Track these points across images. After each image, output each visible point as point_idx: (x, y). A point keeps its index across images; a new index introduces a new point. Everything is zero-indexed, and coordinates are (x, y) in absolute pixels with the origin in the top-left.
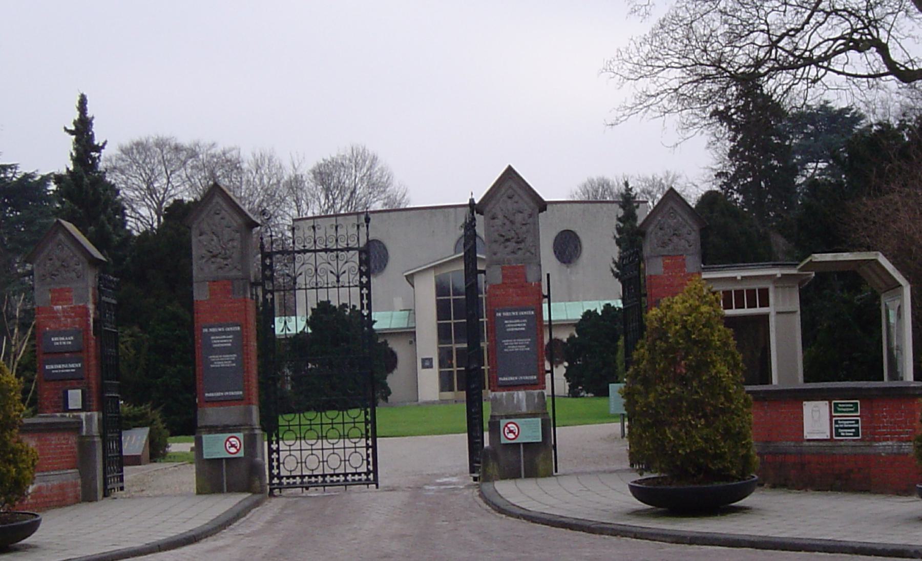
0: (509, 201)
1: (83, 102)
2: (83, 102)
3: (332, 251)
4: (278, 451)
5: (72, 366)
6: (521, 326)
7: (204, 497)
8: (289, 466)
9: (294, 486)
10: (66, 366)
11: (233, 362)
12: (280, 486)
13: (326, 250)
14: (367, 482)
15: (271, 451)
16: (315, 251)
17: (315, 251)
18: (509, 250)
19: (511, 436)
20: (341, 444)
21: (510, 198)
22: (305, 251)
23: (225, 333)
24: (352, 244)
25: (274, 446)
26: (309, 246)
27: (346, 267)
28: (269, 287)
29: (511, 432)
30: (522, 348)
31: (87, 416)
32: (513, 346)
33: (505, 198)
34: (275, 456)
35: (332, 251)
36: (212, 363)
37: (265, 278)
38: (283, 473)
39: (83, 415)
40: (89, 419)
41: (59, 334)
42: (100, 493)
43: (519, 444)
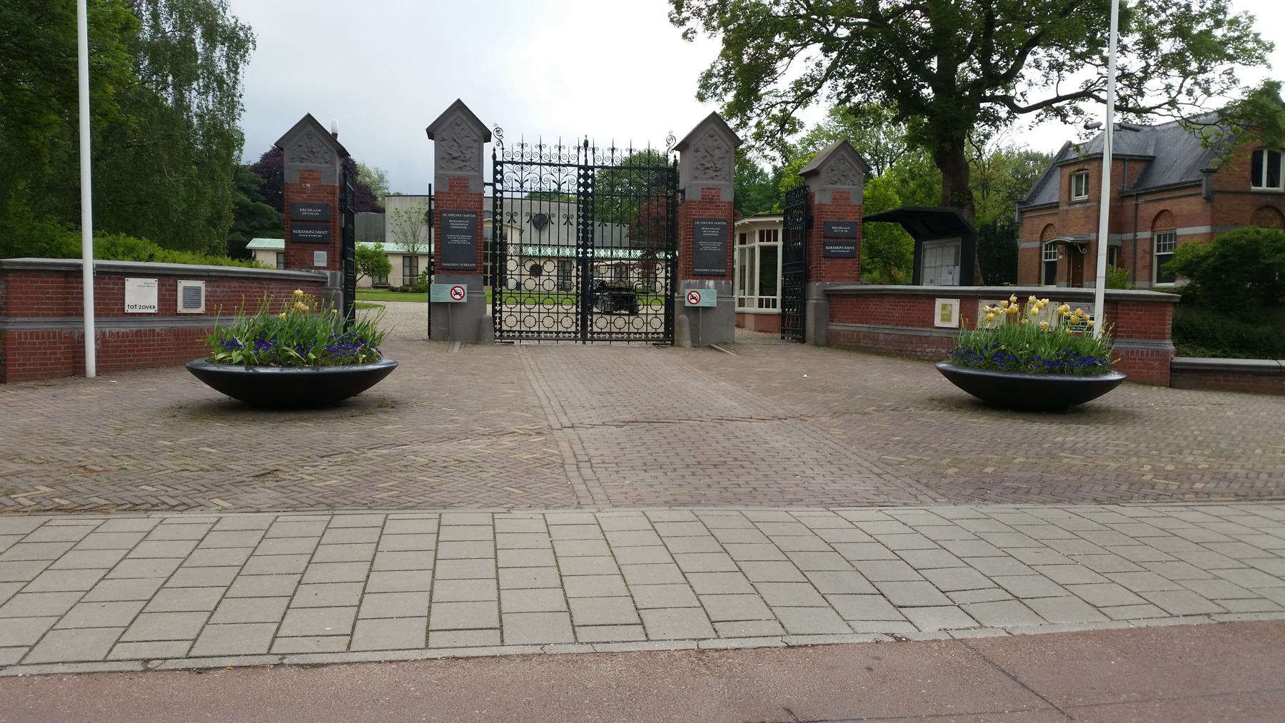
1: (1269, 67)
2: (1269, 67)
3: (517, 163)
4: (501, 311)
6: (463, 225)
7: (435, 344)
8: (510, 322)
9: (622, 340)
13: (550, 164)
14: (576, 339)
15: (494, 311)
16: (541, 164)
17: (541, 164)
22: (531, 163)
23: (462, 218)
24: (573, 162)
25: (498, 308)
26: (536, 160)
27: (566, 179)
28: (499, 186)
30: (715, 249)
32: (706, 246)
34: (498, 315)
35: (517, 163)
37: (495, 180)
38: (573, 329)
39: (328, 273)
41: (837, 224)
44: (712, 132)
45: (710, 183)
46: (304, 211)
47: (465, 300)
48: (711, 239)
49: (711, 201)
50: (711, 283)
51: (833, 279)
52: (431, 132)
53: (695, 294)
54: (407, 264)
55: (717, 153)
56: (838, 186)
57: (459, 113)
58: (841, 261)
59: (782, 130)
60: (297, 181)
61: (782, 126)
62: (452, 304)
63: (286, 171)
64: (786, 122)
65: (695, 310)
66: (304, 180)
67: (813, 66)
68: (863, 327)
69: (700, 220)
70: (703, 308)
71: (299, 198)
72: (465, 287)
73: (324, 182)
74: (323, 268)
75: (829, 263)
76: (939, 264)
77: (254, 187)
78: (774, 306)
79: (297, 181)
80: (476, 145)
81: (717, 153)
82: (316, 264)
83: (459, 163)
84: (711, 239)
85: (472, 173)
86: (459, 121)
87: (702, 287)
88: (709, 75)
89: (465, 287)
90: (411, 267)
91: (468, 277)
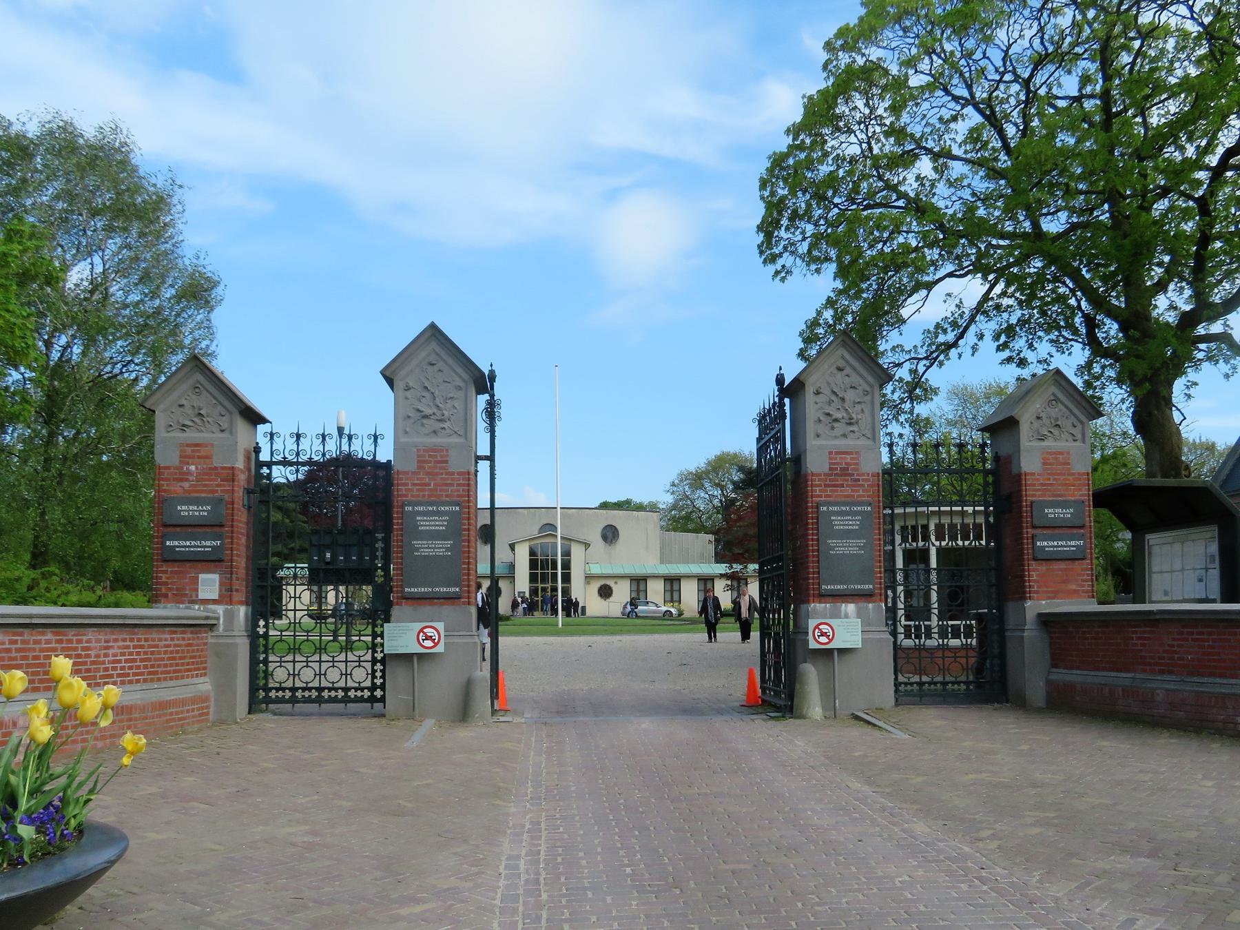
0: (839, 374)
5: (208, 543)
6: (439, 524)
9: (309, 700)
10: (1064, 543)
11: (447, 549)
12: (268, 700)
18: (837, 432)
19: (823, 639)
20: (342, 657)
21: (840, 369)
23: (438, 513)
29: (823, 634)
30: (854, 550)
31: (226, 611)
33: (833, 369)
36: (417, 549)
38: (368, 683)
39: (220, 609)
40: (230, 616)
42: (1064, 676)
43: (831, 650)
44: (841, 363)
45: (842, 443)
46: (186, 510)
47: (440, 649)
48: (847, 534)
49: (845, 472)
50: (851, 608)
51: (1054, 595)
52: (389, 377)
53: (824, 628)
54: (668, 588)
55: (850, 395)
56: (1048, 443)
57: (433, 345)
58: (1062, 565)
59: (912, 398)
60: (177, 463)
61: (911, 392)
62: (420, 656)
63: (158, 448)
64: (917, 389)
65: (827, 654)
66: (185, 459)
67: (953, 308)
68: (1123, 678)
69: (828, 504)
70: (842, 651)
71: (177, 488)
72: (440, 626)
73: (216, 463)
74: (214, 602)
75: (1043, 568)
76: (1178, 566)
77: (291, 505)
78: (928, 636)
79: (177, 463)
80: (461, 394)
81: (850, 395)
82: (202, 595)
83: (431, 424)
84: (847, 534)
85: (455, 440)
86: (433, 358)
87: (836, 615)
88: (814, 323)
89: (440, 626)
90: (672, 591)
91: (447, 610)
